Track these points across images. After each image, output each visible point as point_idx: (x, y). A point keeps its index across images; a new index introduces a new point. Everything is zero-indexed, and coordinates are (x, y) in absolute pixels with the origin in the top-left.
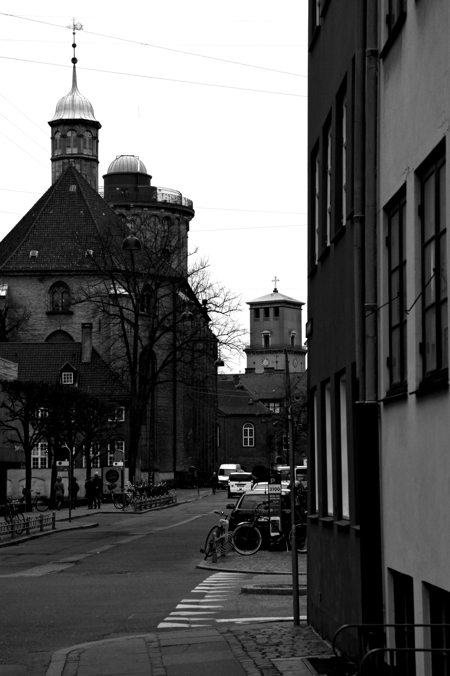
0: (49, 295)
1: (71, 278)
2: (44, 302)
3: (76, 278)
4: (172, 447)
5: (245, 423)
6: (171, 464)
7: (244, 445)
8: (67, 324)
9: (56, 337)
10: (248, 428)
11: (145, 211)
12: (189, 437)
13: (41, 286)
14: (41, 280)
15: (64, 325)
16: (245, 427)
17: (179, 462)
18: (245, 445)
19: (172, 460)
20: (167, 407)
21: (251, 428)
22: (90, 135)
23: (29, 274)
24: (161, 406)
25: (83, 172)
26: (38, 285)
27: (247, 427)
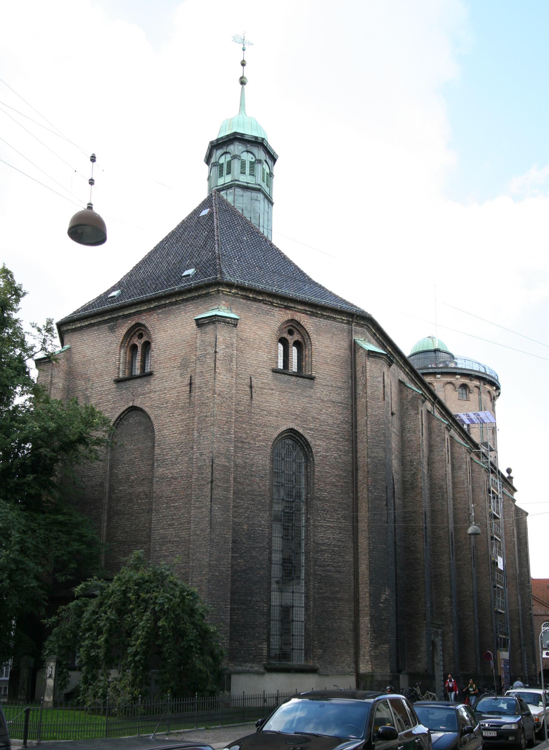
0: (122, 351)
1: (153, 314)
3: (160, 313)
4: (351, 625)
6: (350, 659)
9: (128, 421)
11: (438, 378)
12: (381, 605)
14: (112, 330)
17: (364, 656)
19: (352, 651)
20: (339, 546)
22: (252, 158)
23: (96, 321)
24: (323, 544)
25: (236, 205)
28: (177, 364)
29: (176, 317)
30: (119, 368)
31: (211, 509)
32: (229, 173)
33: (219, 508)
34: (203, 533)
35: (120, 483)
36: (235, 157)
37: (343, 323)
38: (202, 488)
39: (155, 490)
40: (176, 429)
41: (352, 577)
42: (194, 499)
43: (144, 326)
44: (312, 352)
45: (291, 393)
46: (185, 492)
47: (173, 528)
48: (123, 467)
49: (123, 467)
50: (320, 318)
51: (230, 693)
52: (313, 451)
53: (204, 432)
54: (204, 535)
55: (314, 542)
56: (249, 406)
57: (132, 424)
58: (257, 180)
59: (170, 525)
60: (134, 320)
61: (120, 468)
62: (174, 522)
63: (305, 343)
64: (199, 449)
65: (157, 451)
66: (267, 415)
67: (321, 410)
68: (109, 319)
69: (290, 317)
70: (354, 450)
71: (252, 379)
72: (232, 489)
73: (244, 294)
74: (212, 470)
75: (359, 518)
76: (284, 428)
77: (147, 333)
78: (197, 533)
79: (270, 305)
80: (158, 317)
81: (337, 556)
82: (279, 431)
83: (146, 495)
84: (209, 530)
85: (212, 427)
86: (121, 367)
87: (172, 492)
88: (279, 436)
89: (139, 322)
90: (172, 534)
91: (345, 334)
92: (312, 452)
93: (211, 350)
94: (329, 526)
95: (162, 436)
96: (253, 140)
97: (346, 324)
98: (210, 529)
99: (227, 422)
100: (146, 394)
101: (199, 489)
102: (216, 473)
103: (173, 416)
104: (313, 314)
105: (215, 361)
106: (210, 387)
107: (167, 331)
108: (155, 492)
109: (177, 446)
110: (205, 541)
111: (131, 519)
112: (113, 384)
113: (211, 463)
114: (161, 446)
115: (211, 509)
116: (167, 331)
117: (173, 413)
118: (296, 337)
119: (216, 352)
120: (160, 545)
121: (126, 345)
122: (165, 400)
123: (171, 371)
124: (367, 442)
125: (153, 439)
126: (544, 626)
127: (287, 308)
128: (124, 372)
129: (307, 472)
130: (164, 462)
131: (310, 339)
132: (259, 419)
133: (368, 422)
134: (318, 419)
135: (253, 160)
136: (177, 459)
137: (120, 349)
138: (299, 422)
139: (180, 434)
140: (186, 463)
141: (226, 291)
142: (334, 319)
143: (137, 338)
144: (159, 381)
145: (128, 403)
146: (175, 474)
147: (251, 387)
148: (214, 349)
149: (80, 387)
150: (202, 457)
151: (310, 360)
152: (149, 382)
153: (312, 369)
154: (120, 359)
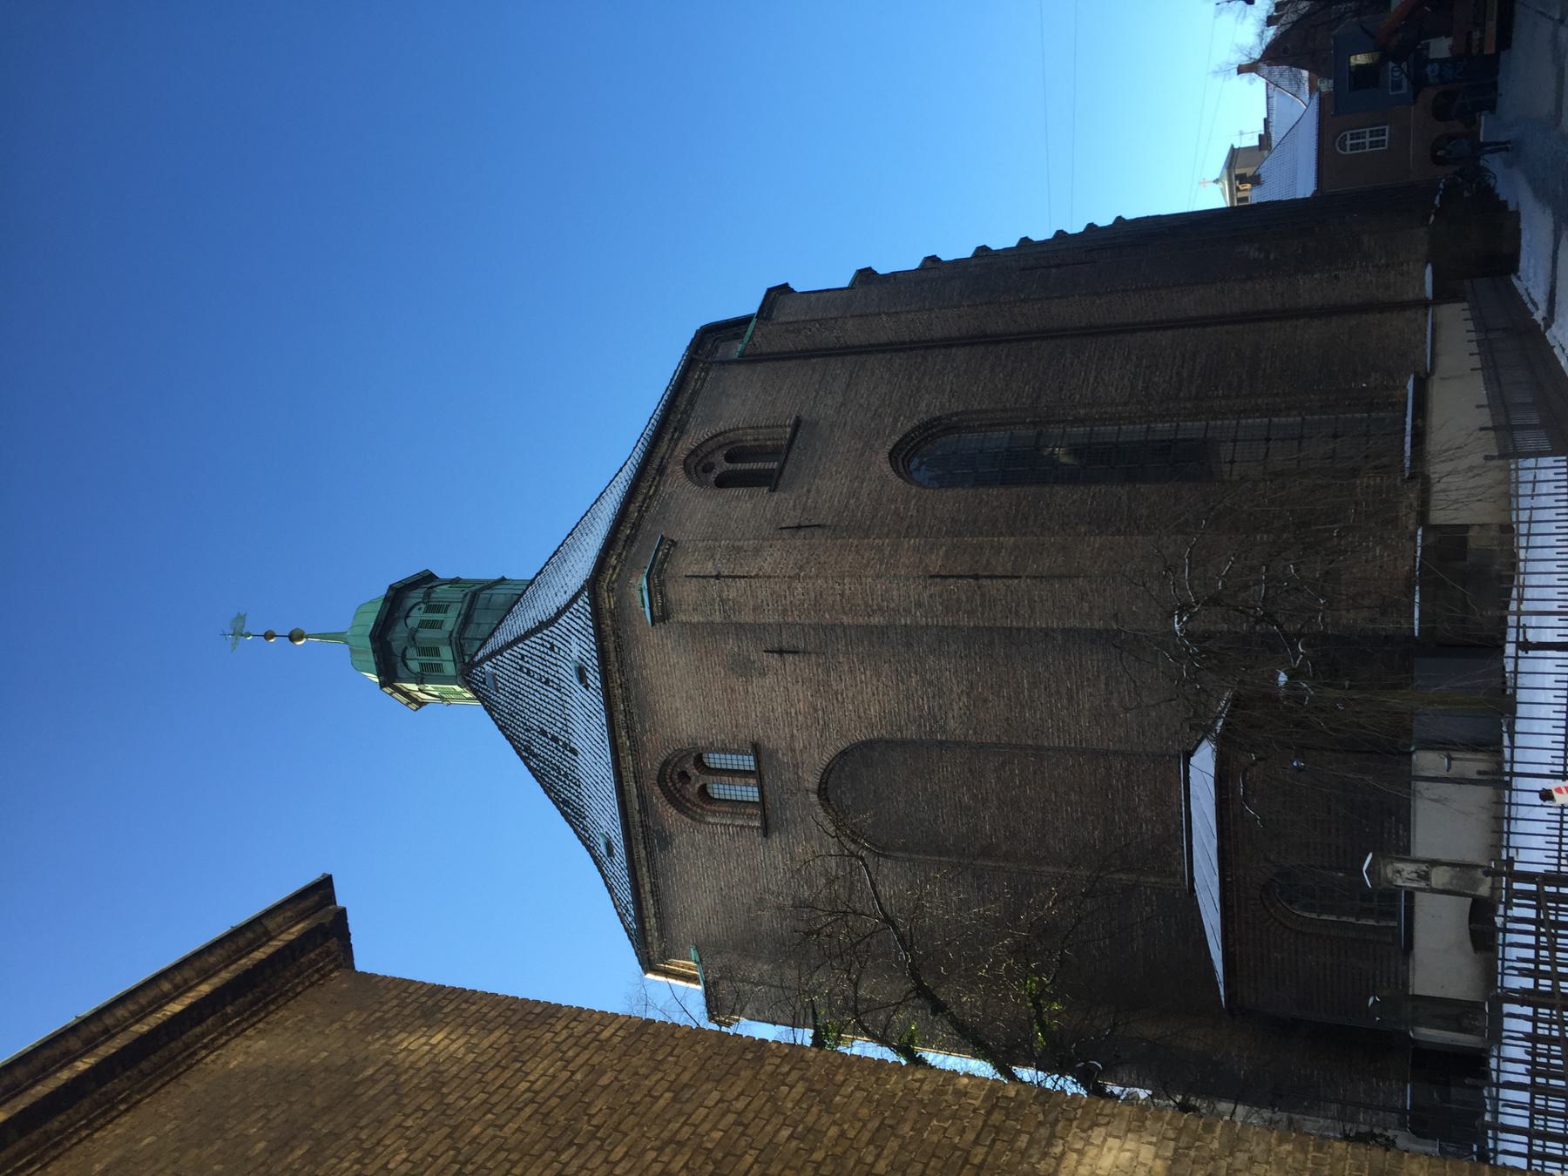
0: (711, 820)
1: (643, 744)
2: (732, 838)
5: (1334, 144)
7: (1385, 148)
8: (796, 766)
10: (1349, 142)
12: (1272, 257)
13: (681, 840)
14: (666, 842)
15: (799, 777)
16: (1345, 150)
18: (1384, 146)
21: (1348, 137)
22: (420, 609)
26: (679, 853)
27: (1346, 145)
28: (739, 684)
29: (652, 690)
30: (742, 827)
31: (1035, 577)
32: (437, 652)
33: (1034, 562)
34: (1087, 595)
35: (977, 831)
36: (412, 638)
37: (705, 379)
38: (989, 601)
39: (994, 738)
40: (869, 686)
41: (1209, 330)
42: (1011, 621)
43: (665, 763)
44: (750, 428)
45: (820, 459)
46: (1001, 662)
47: (1078, 693)
48: (944, 822)
49: (944, 822)
50: (689, 416)
51: (1473, 525)
52: (938, 414)
53: (873, 599)
54: (1092, 591)
55: (1126, 404)
56: (835, 530)
57: (854, 799)
58: (456, 594)
59: (1070, 699)
60: (653, 790)
61: (944, 830)
62: (1064, 691)
63: (733, 442)
64: (907, 611)
65: (911, 732)
66: (858, 499)
67: (861, 406)
68: (645, 848)
69: (679, 468)
70: (948, 343)
71: (784, 526)
72: (996, 539)
73: (621, 543)
74: (952, 577)
75: (1083, 324)
76: (887, 468)
77: (679, 760)
78: (1087, 609)
79: (650, 502)
80: (650, 730)
81: (1161, 360)
82: (892, 475)
83: (1003, 765)
84: (1081, 579)
85: (864, 579)
86: (740, 822)
87: (998, 697)
88: (901, 476)
89: (656, 777)
90: (1091, 695)
91: (726, 374)
92: (940, 417)
93: (714, 587)
94: (1096, 377)
95: (881, 721)
96: (389, 604)
97: (707, 374)
98: (1078, 577)
99: (857, 552)
100: (796, 759)
101: (991, 609)
102: (959, 570)
103: (842, 695)
104: (681, 429)
105: (734, 577)
106: (785, 586)
107: (677, 710)
108: (999, 738)
109: (903, 683)
110: (1104, 590)
111: (1055, 803)
112: (772, 841)
113: (938, 580)
114: (902, 722)
115: (1035, 577)
116: (677, 710)
117: (836, 693)
118: (719, 458)
119: (717, 577)
120: (1114, 725)
121: (699, 811)
122: (809, 713)
123: (754, 699)
124: (931, 310)
125: (888, 744)
126: (1345, 150)
127: (661, 471)
128: (750, 816)
129: (980, 426)
130: (934, 717)
131: (726, 432)
132: (863, 512)
133: (893, 310)
134: (876, 410)
135: (423, 606)
136: (930, 683)
137: (705, 823)
138: (880, 441)
139: (878, 675)
140: (939, 659)
141: (612, 576)
142: (695, 393)
143: (688, 786)
144: (771, 729)
145: (811, 804)
146: (961, 687)
147: (799, 527)
148: (712, 581)
149: (775, 923)
150: (924, 603)
151: (765, 431)
152: (773, 754)
153: (781, 426)
154: (725, 825)
